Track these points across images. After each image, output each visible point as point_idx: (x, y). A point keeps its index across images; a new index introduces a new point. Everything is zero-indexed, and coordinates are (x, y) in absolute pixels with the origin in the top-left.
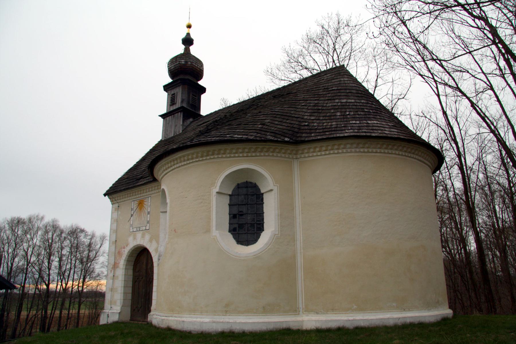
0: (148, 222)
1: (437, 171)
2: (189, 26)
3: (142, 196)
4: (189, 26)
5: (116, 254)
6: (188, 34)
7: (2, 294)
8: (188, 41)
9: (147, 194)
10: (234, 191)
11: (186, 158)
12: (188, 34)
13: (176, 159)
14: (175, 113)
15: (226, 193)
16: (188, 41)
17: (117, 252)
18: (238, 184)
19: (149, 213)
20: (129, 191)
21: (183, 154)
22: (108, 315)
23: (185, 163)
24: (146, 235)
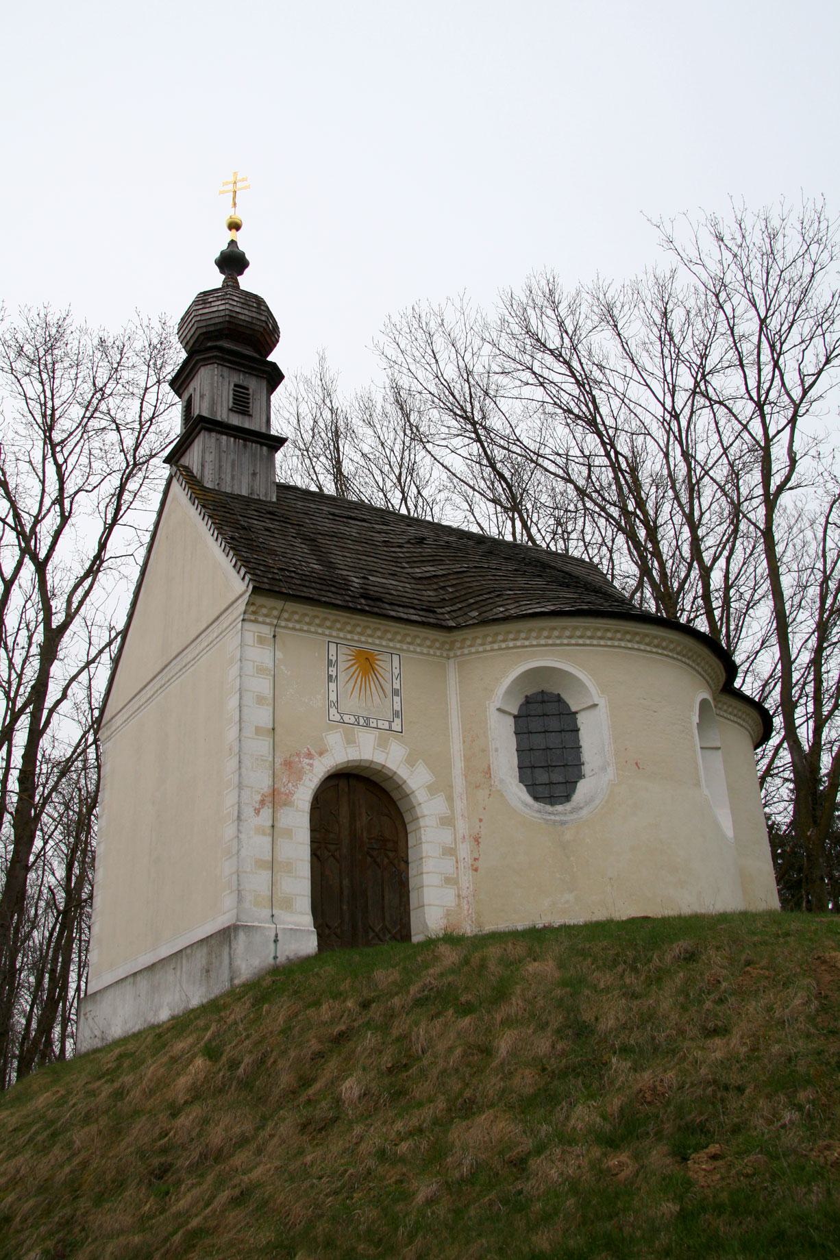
0: (397, 714)
1: (794, 776)
2: (235, 226)
3: (384, 646)
4: (235, 226)
5: (277, 766)
6: (233, 243)
7: (838, 810)
8: (232, 262)
9: (391, 644)
10: (520, 709)
11: (656, 642)
12: (233, 243)
13: (637, 634)
14: (253, 442)
15: (109, 673)
16: (232, 262)
17: (278, 761)
18: (527, 697)
19: (396, 692)
20: (343, 616)
21: (664, 634)
22: (276, 936)
23: (648, 648)
24: (393, 743)
